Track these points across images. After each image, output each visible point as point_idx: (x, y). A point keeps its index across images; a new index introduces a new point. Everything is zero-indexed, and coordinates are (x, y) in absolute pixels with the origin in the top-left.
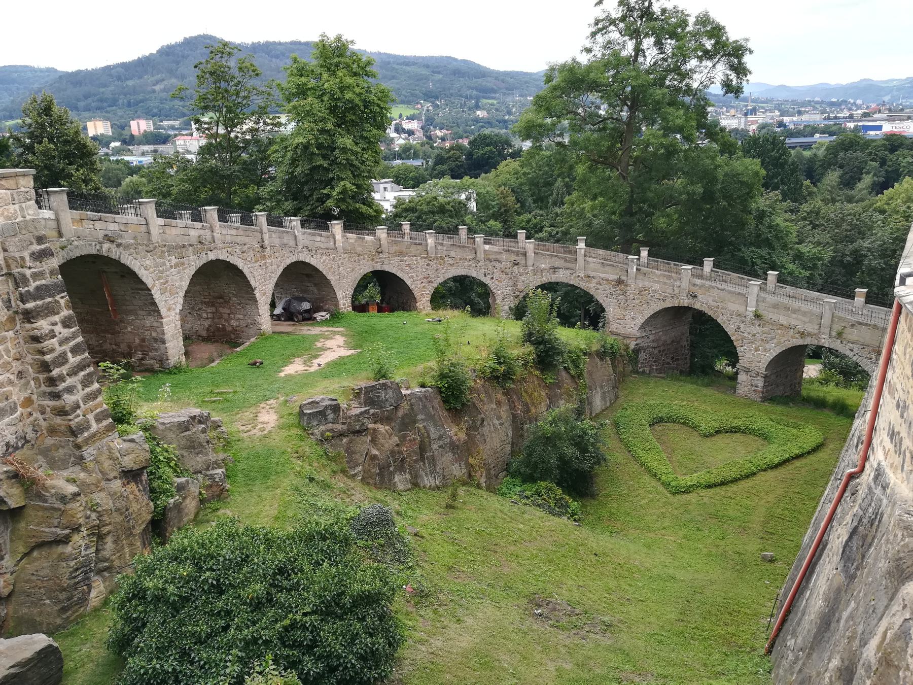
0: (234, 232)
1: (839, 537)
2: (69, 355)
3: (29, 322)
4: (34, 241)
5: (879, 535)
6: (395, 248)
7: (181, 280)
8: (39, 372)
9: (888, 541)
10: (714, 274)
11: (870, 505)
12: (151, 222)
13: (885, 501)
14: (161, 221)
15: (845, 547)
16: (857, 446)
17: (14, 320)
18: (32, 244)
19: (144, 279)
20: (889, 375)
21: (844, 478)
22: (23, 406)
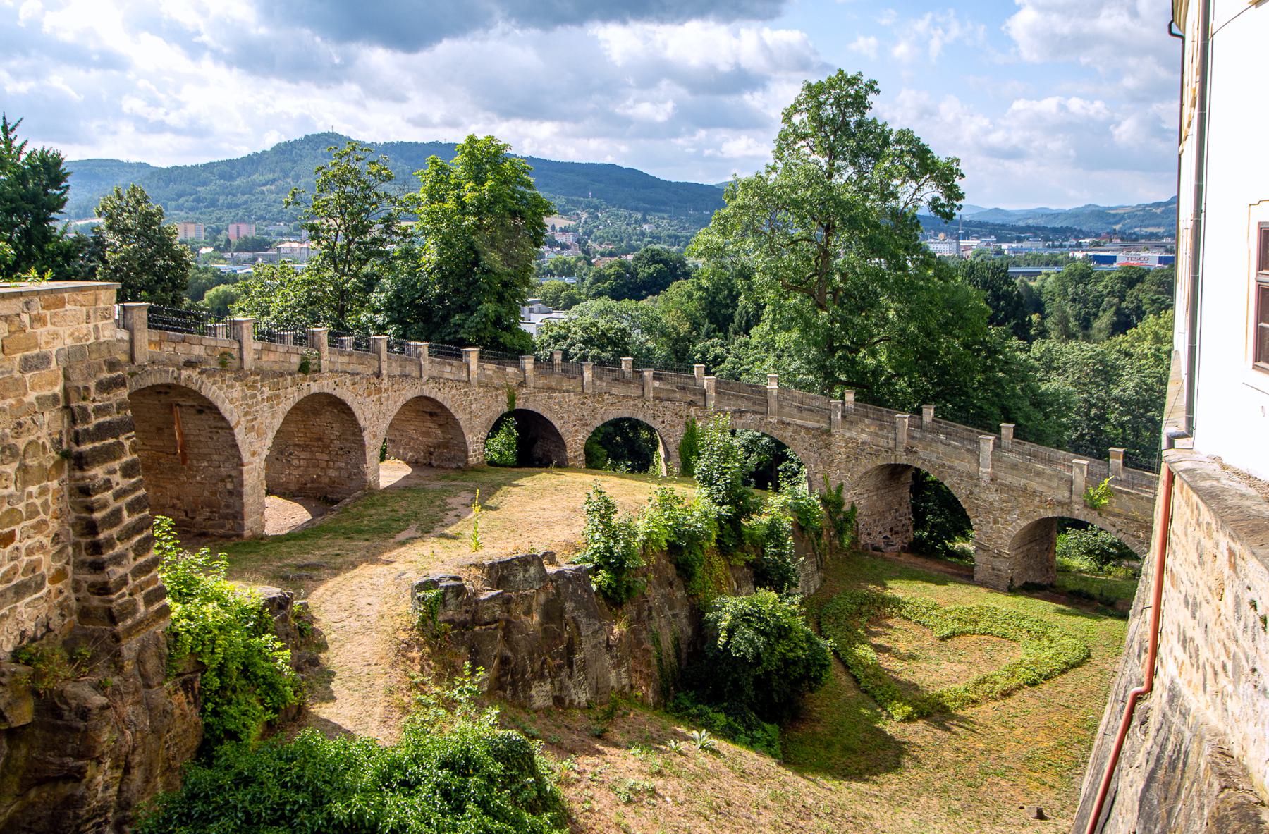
0: (345, 359)
1: (1130, 786)
2: (125, 513)
3: (81, 469)
4: (105, 368)
5: (1187, 784)
6: (541, 382)
7: (272, 419)
8: (82, 535)
9: (1200, 792)
10: (936, 425)
11: (1168, 739)
12: (245, 345)
13: (1187, 734)
14: (258, 345)
15: (1141, 801)
16: (1139, 656)
17: (62, 466)
18: (101, 370)
19: (227, 415)
20: (1169, 561)
21: (1129, 701)
22: (53, 581)
